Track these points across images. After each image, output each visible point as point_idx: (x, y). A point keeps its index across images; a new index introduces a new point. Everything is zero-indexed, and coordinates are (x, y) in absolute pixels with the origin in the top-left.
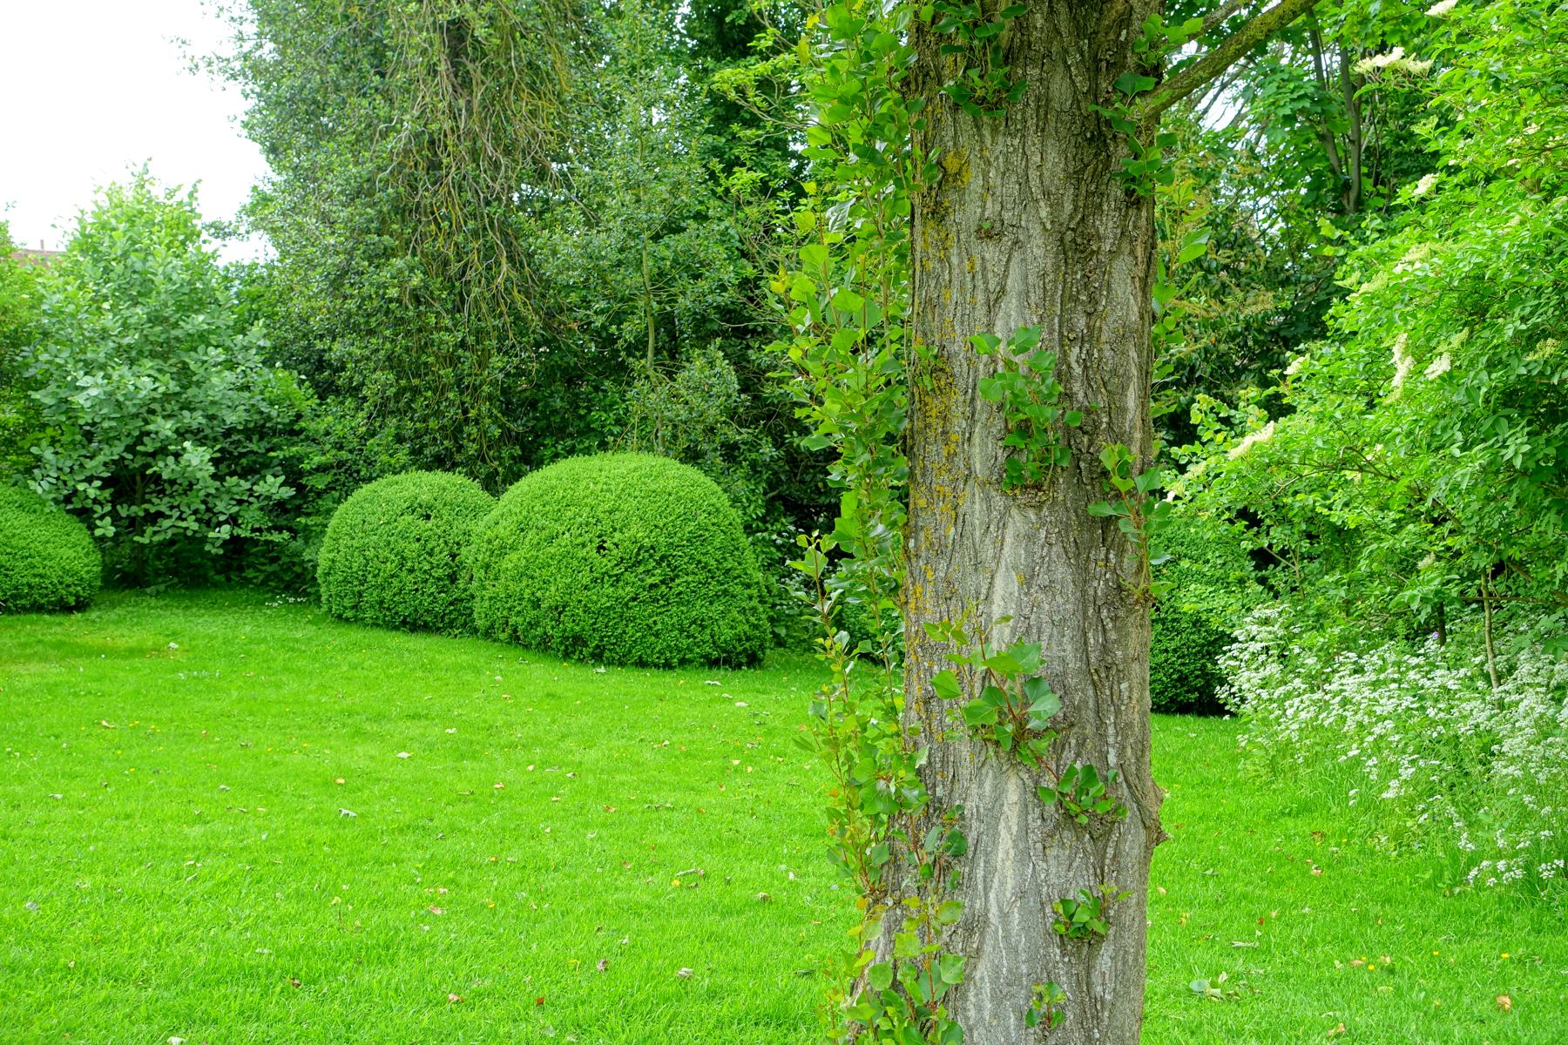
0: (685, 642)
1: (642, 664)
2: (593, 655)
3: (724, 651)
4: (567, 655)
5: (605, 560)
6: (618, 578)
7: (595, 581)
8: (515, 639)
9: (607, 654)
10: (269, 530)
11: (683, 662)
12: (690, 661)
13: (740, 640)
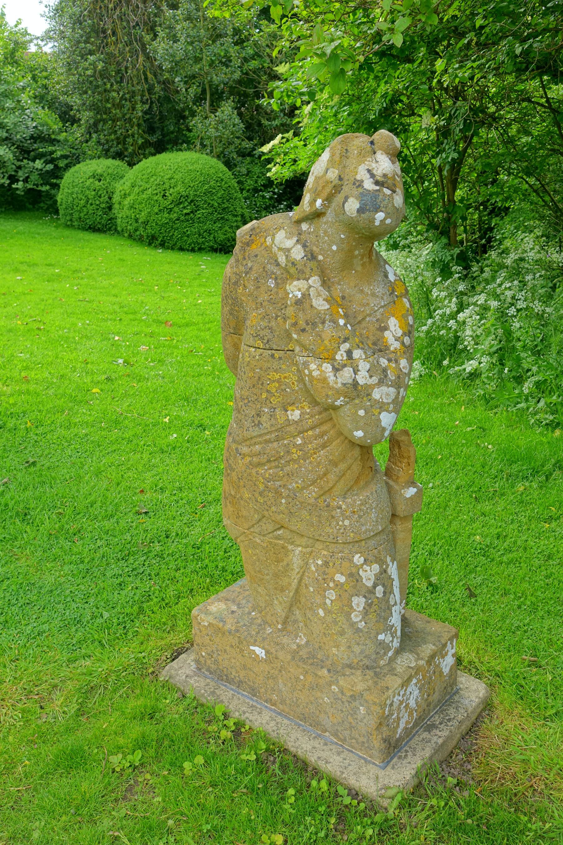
0: (201, 240)
1: (181, 249)
2: (161, 245)
3: (220, 245)
4: (150, 244)
5: (165, 202)
6: (171, 210)
7: (160, 211)
8: (130, 236)
9: (166, 244)
10: (41, 185)
11: (200, 249)
12: (204, 249)
13: (229, 240)
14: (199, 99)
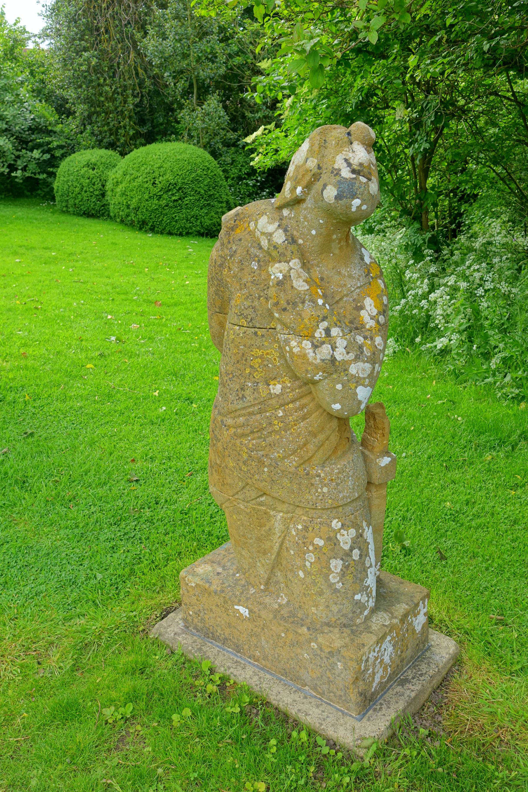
0: (188, 225)
1: (170, 234)
2: (151, 229)
3: (206, 229)
4: (140, 229)
5: (155, 189)
6: (160, 196)
7: (150, 197)
8: (122, 221)
9: (156, 229)
10: (39, 173)
11: (188, 234)
12: (191, 233)
13: (215, 225)
14: (187, 93)
